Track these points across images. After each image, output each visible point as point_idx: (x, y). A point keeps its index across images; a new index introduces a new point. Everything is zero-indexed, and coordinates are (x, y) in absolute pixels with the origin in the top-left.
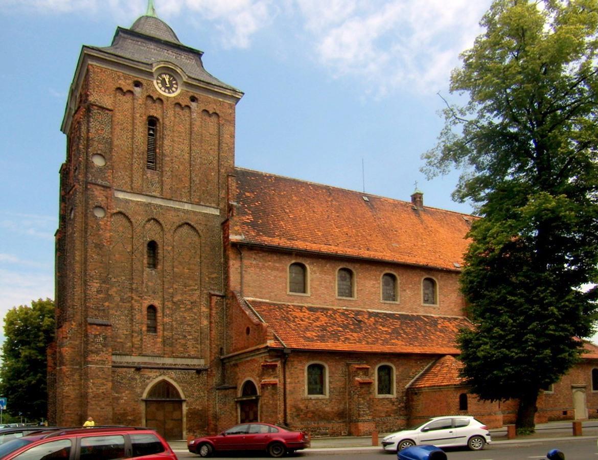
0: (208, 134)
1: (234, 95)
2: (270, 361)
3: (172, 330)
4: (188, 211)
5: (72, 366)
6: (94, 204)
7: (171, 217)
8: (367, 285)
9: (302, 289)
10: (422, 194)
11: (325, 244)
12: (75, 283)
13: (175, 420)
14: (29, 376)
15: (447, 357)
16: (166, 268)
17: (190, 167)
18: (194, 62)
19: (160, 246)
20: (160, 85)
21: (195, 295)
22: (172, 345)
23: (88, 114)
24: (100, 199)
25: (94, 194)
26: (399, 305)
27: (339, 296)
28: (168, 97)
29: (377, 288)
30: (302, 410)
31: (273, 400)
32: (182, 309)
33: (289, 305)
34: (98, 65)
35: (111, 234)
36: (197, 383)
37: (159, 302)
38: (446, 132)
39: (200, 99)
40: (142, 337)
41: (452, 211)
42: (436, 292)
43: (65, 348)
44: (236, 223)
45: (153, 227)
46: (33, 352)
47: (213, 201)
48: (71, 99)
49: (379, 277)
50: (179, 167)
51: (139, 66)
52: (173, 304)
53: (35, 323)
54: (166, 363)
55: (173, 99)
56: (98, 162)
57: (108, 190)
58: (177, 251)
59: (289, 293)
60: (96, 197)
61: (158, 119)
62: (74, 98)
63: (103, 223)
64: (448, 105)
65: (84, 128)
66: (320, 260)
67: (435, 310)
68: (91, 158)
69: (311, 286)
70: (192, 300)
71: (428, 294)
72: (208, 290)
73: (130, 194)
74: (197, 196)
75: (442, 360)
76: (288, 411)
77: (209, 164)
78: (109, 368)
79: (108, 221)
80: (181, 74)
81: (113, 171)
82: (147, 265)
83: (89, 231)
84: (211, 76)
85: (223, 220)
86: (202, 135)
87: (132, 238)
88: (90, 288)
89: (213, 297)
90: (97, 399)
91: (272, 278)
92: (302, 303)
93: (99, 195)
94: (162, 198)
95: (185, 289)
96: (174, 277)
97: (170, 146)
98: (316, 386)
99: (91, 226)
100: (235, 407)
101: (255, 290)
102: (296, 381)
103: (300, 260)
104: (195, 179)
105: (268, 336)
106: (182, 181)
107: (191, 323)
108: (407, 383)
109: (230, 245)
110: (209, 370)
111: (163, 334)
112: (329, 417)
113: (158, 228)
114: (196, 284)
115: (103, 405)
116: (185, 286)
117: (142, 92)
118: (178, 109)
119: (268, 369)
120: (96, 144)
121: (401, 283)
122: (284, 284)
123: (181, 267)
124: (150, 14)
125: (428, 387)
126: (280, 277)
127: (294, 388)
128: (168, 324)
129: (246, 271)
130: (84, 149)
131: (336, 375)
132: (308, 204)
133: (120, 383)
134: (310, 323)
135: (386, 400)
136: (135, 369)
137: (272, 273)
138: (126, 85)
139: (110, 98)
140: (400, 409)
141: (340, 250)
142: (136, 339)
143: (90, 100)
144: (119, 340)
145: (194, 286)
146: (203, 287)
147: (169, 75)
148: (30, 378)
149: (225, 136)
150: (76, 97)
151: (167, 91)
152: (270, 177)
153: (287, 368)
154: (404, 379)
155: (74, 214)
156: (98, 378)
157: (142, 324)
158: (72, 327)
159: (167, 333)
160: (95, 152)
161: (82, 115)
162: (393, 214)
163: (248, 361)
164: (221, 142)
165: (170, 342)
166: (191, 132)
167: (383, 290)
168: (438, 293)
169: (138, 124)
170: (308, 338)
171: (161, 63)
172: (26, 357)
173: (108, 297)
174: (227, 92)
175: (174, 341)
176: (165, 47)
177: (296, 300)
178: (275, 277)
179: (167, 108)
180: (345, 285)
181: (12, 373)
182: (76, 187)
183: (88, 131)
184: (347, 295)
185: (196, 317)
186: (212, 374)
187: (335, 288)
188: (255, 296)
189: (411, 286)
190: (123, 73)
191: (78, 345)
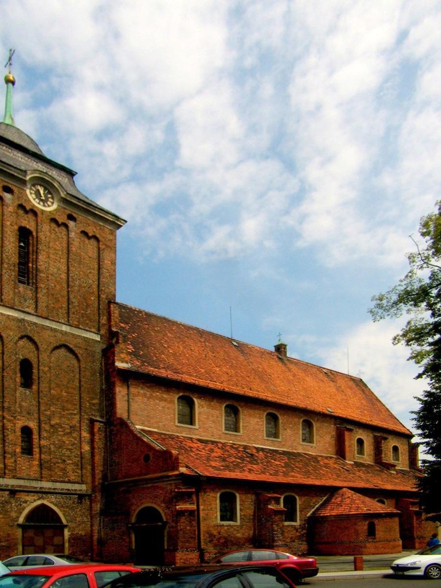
1: (116, 222)
4: (66, 333)
7: (47, 337)
9: (189, 420)
10: (286, 346)
11: (211, 381)
13: (55, 546)
15: (345, 489)
16: (42, 389)
19: (35, 365)
20: (34, 196)
21: (74, 420)
26: (280, 442)
27: (225, 430)
29: (261, 425)
30: (215, 536)
36: (80, 508)
37: (35, 424)
38: (410, 275)
39: (77, 219)
41: (312, 363)
42: (313, 432)
44: (122, 351)
45: (27, 345)
49: (263, 416)
50: (55, 286)
54: (45, 487)
55: (48, 214)
59: (177, 424)
64: (418, 249)
67: (312, 449)
69: (199, 419)
70: (71, 425)
71: (305, 434)
72: (89, 415)
74: (76, 318)
75: (340, 492)
76: (202, 537)
77: (89, 288)
80: (58, 188)
89: (96, 423)
91: (160, 408)
94: (37, 316)
95: (63, 413)
97: (46, 262)
98: (228, 513)
101: (143, 418)
102: (209, 508)
104: (73, 300)
105: (180, 463)
106: (59, 301)
107: (70, 447)
108: (308, 512)
111: (40, 456)
112: (240, 542)
114: (75, 409)
116: (64, 409)
117: (13, 200)
118: (53, 225)
121: (282, 423)
123: (58, 390)
124: (8, 121)
125: (335, 516)
126: (168, 408)
127: (207, 515)
128: (45, 447)
129: (132, 399)
131: (246, 503)
137: (160, 403)
140: (303, 535)
146: (83, 411)
149: (106, 261)
151: (42, 203)
152: (140, 312)
153: (200, 495)
154: (306, 508)
157: (15, 445)
159: (45, 457)
164: (101, 266)
165: (48, 465)
167: (266, 428)
168: (315, 434)
169: (9, 232)
171: (37, 172)
174: (110, 217)
175: (52, 464)
177: (185, 431)
178: (163, 407)
179: (41, 221)
184: (232, 430)
185: (76, 442)
186: (96, 500)
187: (222, 422)
188: (143, 424)
189: (291, 426)
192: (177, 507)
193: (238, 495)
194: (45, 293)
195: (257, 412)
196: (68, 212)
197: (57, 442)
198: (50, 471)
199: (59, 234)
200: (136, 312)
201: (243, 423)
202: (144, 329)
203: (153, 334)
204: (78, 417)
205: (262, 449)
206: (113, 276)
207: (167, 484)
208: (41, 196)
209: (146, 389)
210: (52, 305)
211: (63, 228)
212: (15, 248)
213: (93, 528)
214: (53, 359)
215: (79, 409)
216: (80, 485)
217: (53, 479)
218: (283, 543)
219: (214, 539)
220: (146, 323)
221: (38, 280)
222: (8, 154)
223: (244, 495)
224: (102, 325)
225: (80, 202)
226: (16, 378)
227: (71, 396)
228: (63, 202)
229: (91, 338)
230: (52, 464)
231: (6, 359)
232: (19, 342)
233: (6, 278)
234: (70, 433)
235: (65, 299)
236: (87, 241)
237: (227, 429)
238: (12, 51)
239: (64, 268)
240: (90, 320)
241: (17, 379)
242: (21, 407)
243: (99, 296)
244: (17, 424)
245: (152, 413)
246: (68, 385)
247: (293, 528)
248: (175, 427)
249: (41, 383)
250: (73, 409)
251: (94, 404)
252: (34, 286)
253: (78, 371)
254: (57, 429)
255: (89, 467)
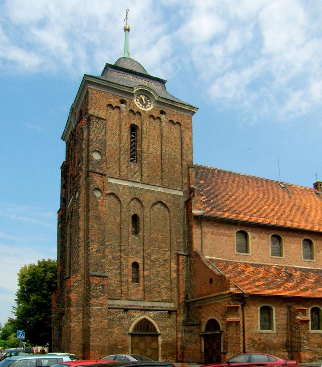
0: (173, 137)
1: (191, 110)
2: (233, 305)
3: (150, 281)
5: (77, 308)
6: (94, 187)
7: (149, 197)
8: (292, 248)
11: (260, 217)
12: (80, 245)
13: (153, 349)
14: (37, 315)
17: (162, 161)
18: (160, 87)
19: (141, 218)
20: (139, 102)
21: (166, 255)
22: (150, 292)
23: (89, 123)
24: (98, 183)
25: (94, 180)
28: (144, 111)
30: (256, 342)
31: (237, 334)
32: (157, 265)
33: (236, 262)
34: (95, 88)
35: (106, 209)
37: (141, 260)
40: (128, 286)
43: (72, 294)
46: (39, 297)
47: (178, 186)
48: (71, 115)
50: (153, 161)
51: (124, 89)
52: (151, 261)
53: (41, 276)
56: (96, 156)
57: (104, 176)
58: (153, 222)
60: (95, 181)
61: (137, 127)
62: (74, 113)
63: (101, 201)
65: (85, 133)
66: (258, 229)
68: (92, 154)
70: (164, 259)
73: (118, 180)
74: (167, 181)
76: (246, 343)
77: (175, 159)
78: (105, 310)
79: (104, 199)
80: (153, 94)
81: (106, 164)
82: (131, 232)
83: (90, 206)
84: (173, 97)
85: (186, 199)
86: (169, 138)
87: (121, 212)
88: (91, 249)
90: (97, 333)
91: (224, 242)
92: (245, 260)
93: (97, 180)
95: (159, 251)
96: (151, 241)
98: (267, 323)
99: (92, 203)
100: (199, 339)
101: (212, 250)
102: (252, 319)
103: (243, 229)
104: (165, 169)
105: (231, 284)
106: (156, 171)
107: (164, 275)
109: (193, 217)
110: (178, 311)
112: (276, 347)
113: (138, 205)
114: (167, 247)
115: (101, 337)
118: (151, 120)
119: (232, 310)
120: (94, 143)
122: (233, 247)
123: (156, 234)
124: (126, 56)
126: (229, 241)
127: (250, 325)
129: (204, 236)
130: (85, 147)
131: (281, 314)
132: (243, 189)
133: (113, 320)
134: (256, 275)
135: (317, 335)
136: (123, 310)
137: (224, 238)
138: (115, 102)
139: (104, 111)
141: (272, 221)
142: (124, 288)
143: (89, 112)
144: (111, 288)
145: (166, 248)
147: (144, 95)
148: (37, 316)
149: (186, 139)
150: (76, 113)
151: (144, 106)
152: (214, 170)
153: (245, 309)
155: (79, 194)
156: (98, 317)
158: (78, 278)
160: (94, 150)
161: (84, 123)
162: (303, 197)
163: (211, 304)
164: (183, 143)
165: (149, 289)
166: (161, 136)
167: (303, 251)
169: (124, 130)
170: (258, 286)
172: (34, 300)
173: (104, 256)
174: (186, 107)
175: (151, 289)
176: (140, 77)
177: (241, 258)
178: (226, 241)
179: (144, 118)
180: (275, 247)
181: (24, 312)
182: (80, 175)
183: (89, 134)
185: (168, 271)
188: (212, 255)
190: (112, 94)
191: (82, 291)
192: (228, 319)
193: (274, 308)
194: (147, 167)
195: (296, 239)
196: (160, 109)
197: (155, 272)
198: (150, 294)
199: (155, 125)
200: (211, 171)
201: (285, 249)
202: (216, 182)
203: (221, 185)
204: (169, 253)
205: (300, 269)
206: (191, 148)
207: (223, 301)
208: (143, 102)
209: (214, 228)
210: (152, 174)
211: (158, 120)
212: (128, 139)
213: (178, 336)
214: (152, 212)
215: (169, 247)
216: (170, 303)
217: (152, 299)
218: (308, 348)
219: (255, 344)
220: (217, 178)
221: (143, 159)
222: (124, 78)
223: (279, 308)
224: (184, 184)
225: (167, 101)
226: (129, 228)
227: (164, 238)
228: (157, 103)
229: (177, 194)
230: (151, 289)
231: (123, 216)
232: (131, 203)
233: (122, 160)
234: (164, 265)
235: (160, 169)
236: (173, 127)
237: (273, 254)
238: (127, 11)
239: (159, 148)
240: (176, 182)
241: (130, 229)
242: (132, 248)
243: (182, 164)
244: (129, 261)
245: (218, 246)
246: (163, 230)
247: (319, 335)
248: (234, 256)
249: (145, 230)
250: (166, 247)
251: (179, 242)
252: (140, 163)
253: (169, 219)
254: (155, 263)
255: (176, 290)
